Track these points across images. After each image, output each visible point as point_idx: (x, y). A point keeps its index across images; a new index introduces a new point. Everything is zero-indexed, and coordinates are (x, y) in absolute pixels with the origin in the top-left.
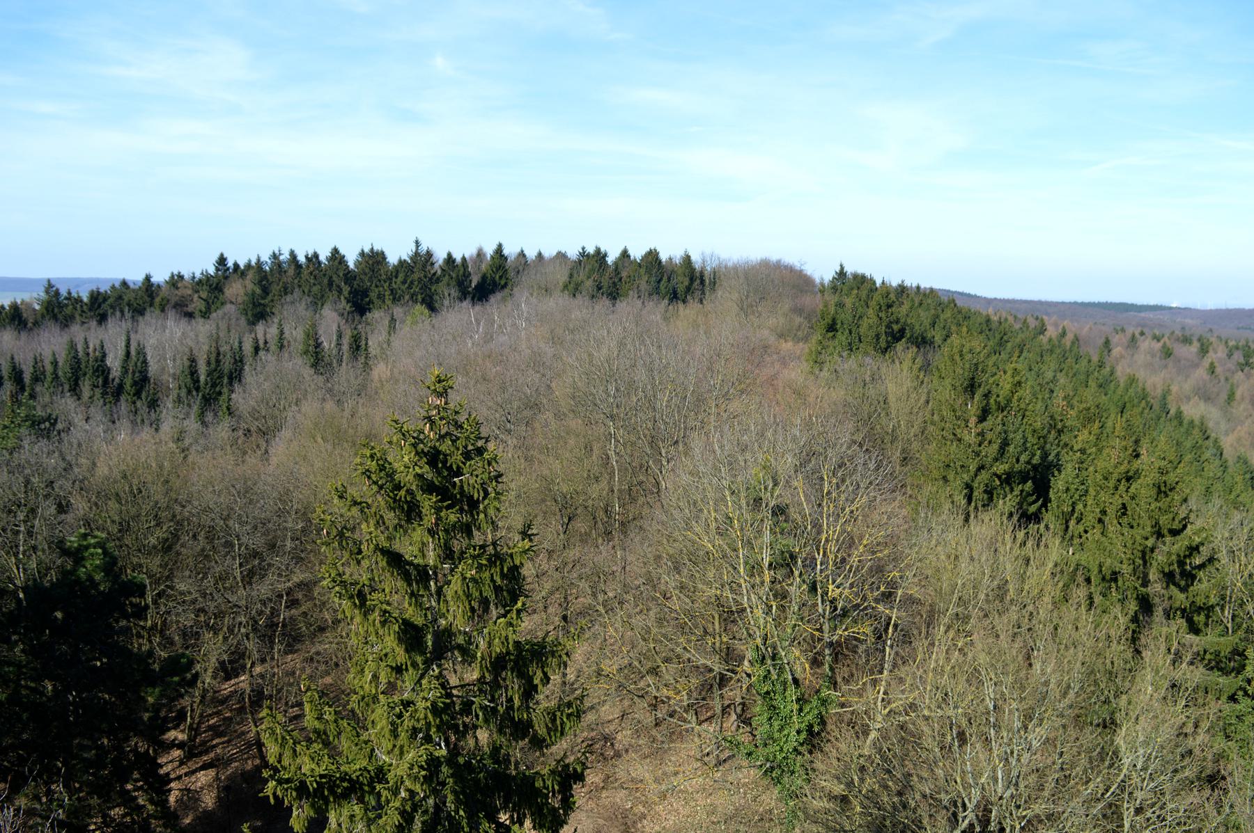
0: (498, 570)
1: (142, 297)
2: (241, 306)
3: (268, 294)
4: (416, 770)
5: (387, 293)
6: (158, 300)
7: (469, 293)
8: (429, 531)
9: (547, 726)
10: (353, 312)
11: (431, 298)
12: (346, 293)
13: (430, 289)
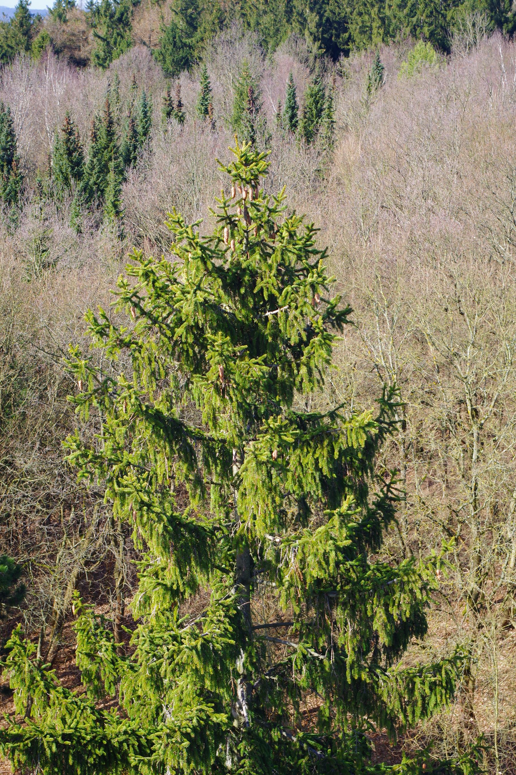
0: (325, 453)
1: (15, 36)
2: (157, 49)
3: (195, 28)
4: (178, 736)
5: (375, 25)
6: (37, 39)
7: (507, 20)
8: (217, 388)
9: (401, 696)
10: (322, 56)
11: (444, 29)
12: (312, 25)
13: (444, 16)
